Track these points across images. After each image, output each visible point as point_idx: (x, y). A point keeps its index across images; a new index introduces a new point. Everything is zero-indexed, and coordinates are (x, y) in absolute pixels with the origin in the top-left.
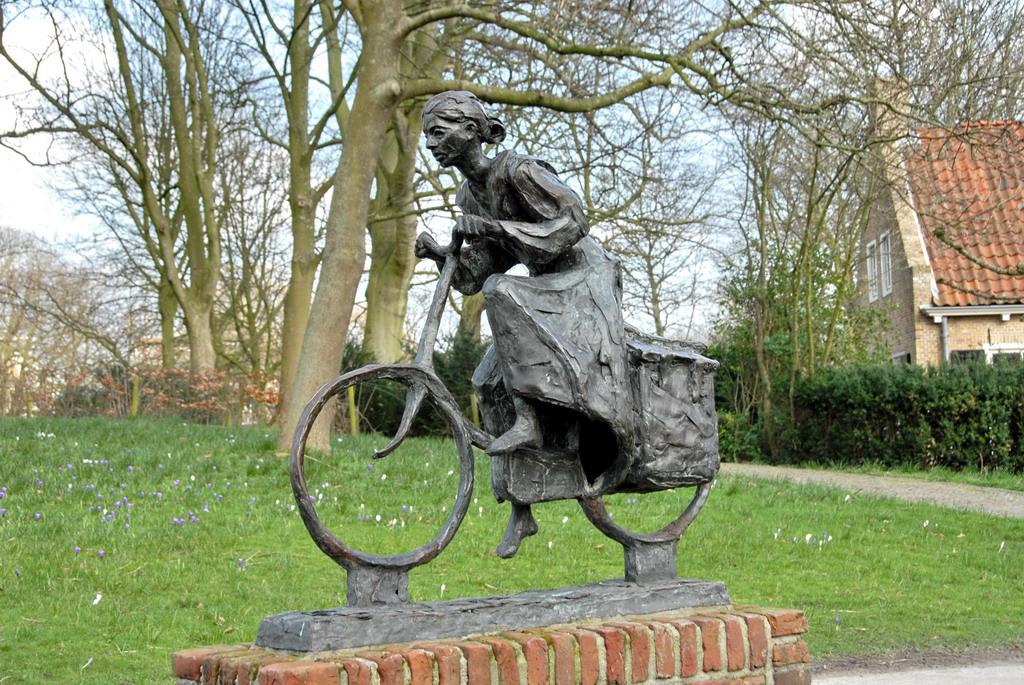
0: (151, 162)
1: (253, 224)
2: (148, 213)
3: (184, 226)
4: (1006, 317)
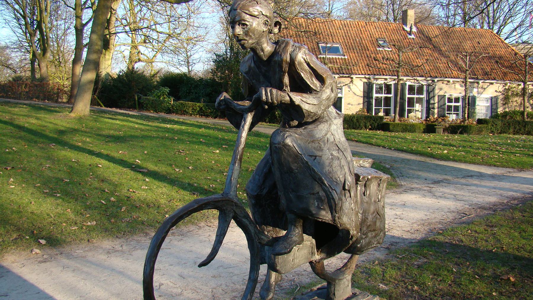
0: (28, 11)
1: (60, 33)
2: (26, 28)
3: (38, 33)
4: (451, 82)
